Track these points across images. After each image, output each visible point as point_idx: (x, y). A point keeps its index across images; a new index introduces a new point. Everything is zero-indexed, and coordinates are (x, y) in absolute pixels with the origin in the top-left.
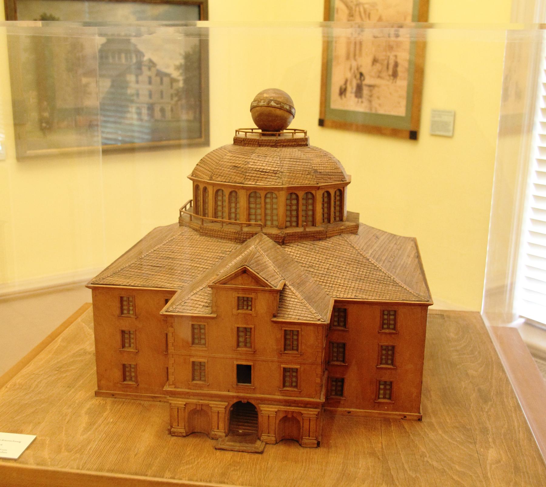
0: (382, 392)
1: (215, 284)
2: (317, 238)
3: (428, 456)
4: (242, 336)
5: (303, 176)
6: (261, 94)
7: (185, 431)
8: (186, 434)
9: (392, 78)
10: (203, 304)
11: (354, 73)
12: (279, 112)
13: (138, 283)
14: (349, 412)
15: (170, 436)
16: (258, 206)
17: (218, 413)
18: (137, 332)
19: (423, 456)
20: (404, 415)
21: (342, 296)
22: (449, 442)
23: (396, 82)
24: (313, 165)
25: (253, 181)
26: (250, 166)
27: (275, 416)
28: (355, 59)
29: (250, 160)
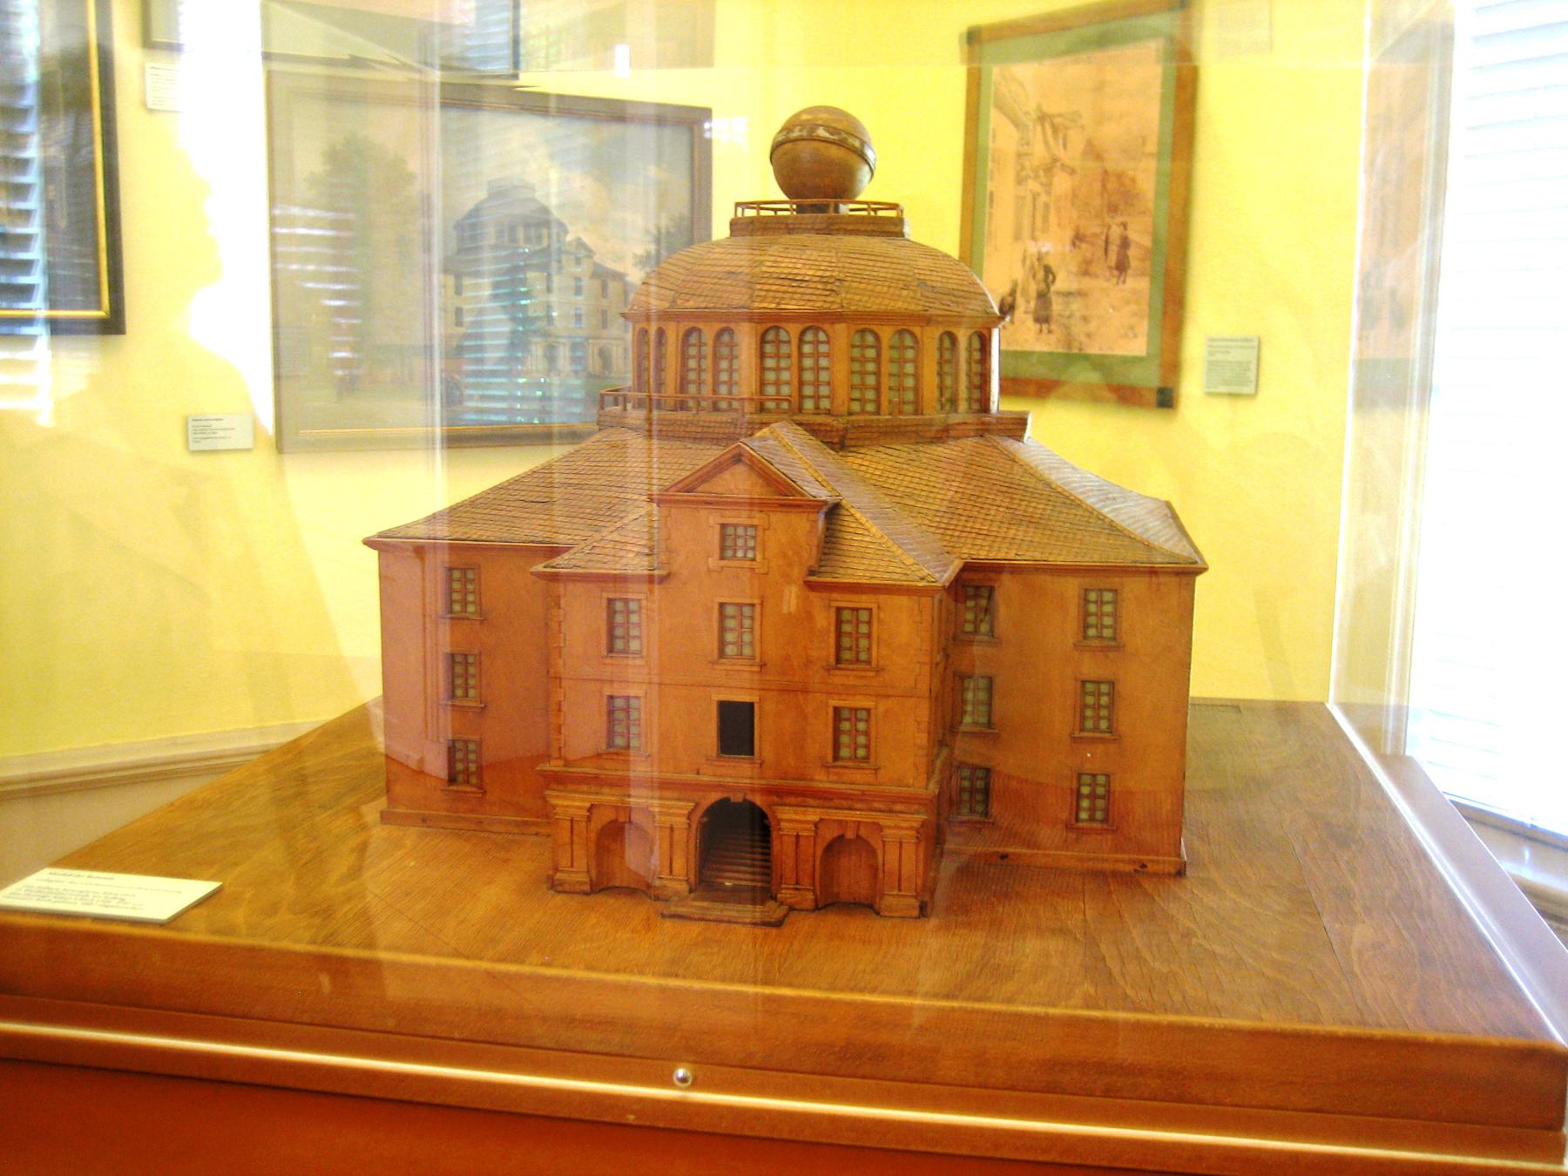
0: (1085, 803)
1: (667, 490)
2: (924, 437)
3: (1199, 934)
4: (732, 630)
5: (891, 290)
6: (797, 116)
7: (588, 880)
8: (591, 887)
9: (1116, 273)
10: (636, 549)
11: (1032, 267)
12: (835, 152)
13: (489, 533)
14: (1004, 856)
15: (552, 892)
16: (783, 364)
17: (672, 829)
18: (483, 658)
19: (1187, 935)
20: (1140, 861)
21: (983, 554)
22: (1255, 913)
23: (1124, 282)
24: (916, 271)
25: (771, 302)
26: (764, 269)
27: (813, 834)
28: (1034, 238)
29: (767, 258)
